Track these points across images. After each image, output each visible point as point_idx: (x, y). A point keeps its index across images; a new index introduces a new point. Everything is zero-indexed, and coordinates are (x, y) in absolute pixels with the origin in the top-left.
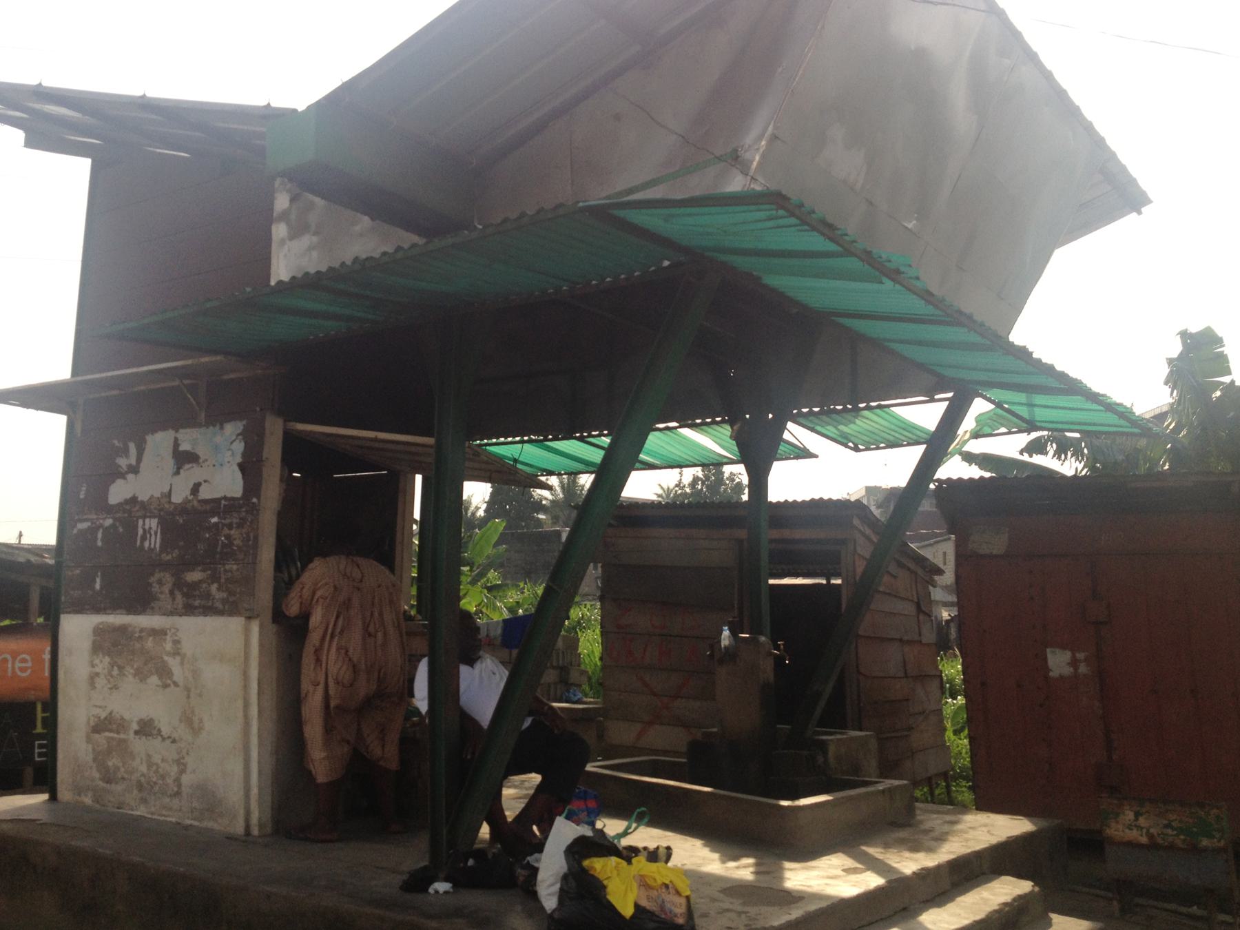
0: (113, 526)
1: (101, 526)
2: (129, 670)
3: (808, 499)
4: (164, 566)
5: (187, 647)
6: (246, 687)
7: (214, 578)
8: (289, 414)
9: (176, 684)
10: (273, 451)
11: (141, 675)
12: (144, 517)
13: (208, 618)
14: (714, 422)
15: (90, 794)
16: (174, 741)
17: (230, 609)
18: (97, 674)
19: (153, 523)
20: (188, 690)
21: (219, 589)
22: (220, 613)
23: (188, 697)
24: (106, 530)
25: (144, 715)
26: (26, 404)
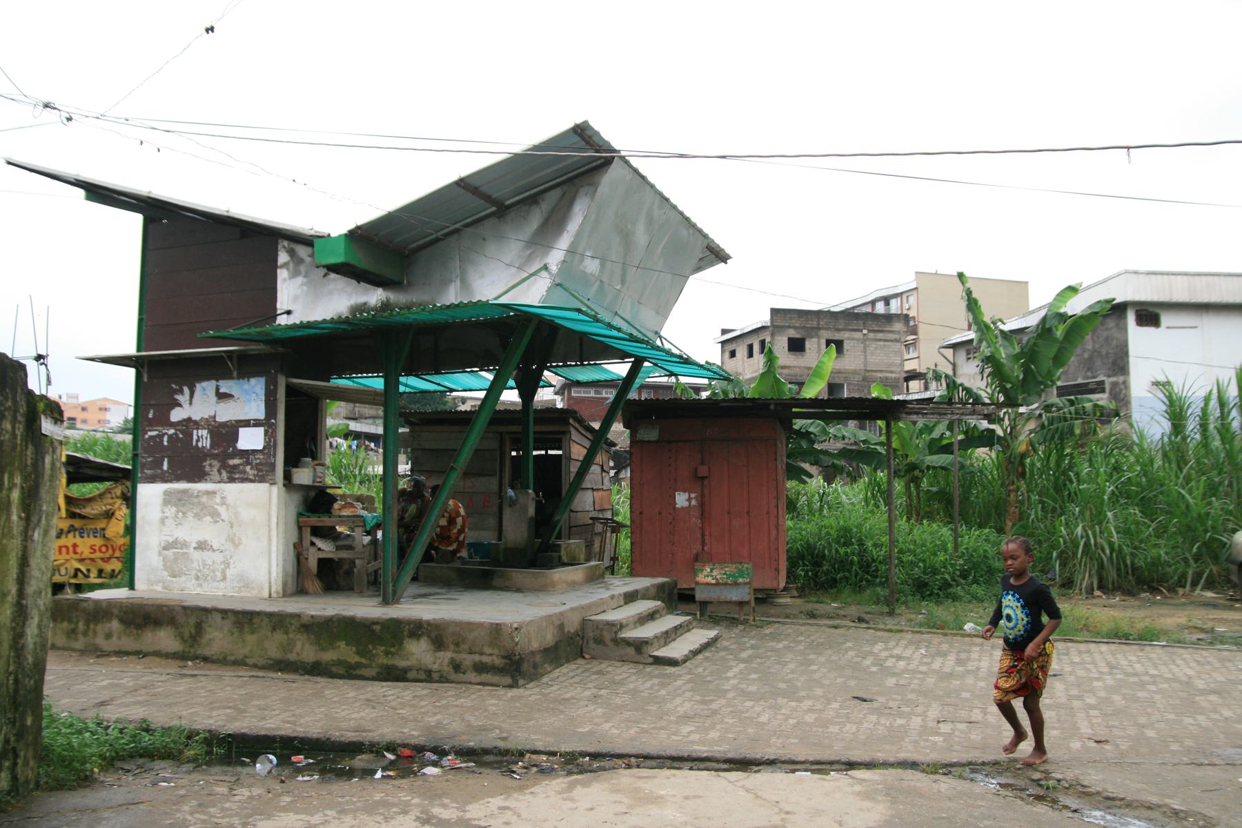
0: (175, 434)
1: (166, 434)
2: (190, 514)
4: (214, 457)
5: (229, 500)
6: (269, 520)
9: (223, 521)
12: (198, 429)
15: (160, 584)
16: (222, 552)
17: (261, 479)
18: (167, 517)
19: (204, 433)
21: (251, 469)
22: (252, 481)
23: (232, 527)
24: (170, 437)
25: (201, 539)
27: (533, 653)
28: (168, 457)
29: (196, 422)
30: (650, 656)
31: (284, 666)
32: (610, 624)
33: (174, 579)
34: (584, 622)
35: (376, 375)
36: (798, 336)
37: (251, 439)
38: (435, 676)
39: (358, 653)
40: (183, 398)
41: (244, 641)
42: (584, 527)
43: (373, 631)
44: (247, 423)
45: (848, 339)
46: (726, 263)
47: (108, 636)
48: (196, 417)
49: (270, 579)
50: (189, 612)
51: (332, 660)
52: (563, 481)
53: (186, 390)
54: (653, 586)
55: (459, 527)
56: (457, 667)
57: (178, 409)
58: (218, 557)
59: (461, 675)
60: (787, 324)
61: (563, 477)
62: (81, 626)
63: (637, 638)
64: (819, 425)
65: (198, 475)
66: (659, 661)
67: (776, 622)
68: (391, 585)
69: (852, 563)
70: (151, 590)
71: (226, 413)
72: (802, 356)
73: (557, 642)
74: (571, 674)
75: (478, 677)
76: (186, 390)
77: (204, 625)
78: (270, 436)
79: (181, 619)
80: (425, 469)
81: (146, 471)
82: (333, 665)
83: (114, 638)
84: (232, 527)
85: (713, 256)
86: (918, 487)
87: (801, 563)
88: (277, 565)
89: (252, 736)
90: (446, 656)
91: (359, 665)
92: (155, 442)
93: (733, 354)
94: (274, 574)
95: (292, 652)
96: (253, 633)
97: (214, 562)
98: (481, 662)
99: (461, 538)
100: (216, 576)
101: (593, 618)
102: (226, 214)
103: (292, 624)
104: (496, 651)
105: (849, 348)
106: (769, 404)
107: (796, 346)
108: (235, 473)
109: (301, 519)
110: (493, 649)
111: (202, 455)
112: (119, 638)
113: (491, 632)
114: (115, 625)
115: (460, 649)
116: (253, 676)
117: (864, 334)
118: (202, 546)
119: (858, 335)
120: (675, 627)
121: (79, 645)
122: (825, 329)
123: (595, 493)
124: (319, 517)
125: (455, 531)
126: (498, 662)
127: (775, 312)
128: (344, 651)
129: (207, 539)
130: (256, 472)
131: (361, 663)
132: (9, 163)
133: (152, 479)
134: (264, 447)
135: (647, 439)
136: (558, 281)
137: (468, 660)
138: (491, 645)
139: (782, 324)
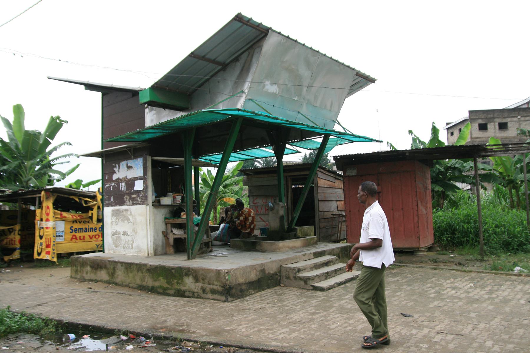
0: (115, 185)
1: (112, 185)
2: (120, 220)
3: (365, 153)
4: (127, 194)
5: (133, 213)
6: (147, 221)
7: (138, 196)
8: (152, 155)
9: (131, 222)
10: (149, 164)
11: (123, 221)
12: (121, 182)
13: (137, 206)
14: (268, 146)
15: (112, 250)
16: (131, 236)
17: (143, 203)
18: (113, 221)
19: (123, 184)
20: (134, 223)
21: (139, 199)
22: (140, 204)
23: (134, 225)
24: (113, 186)
25: (124, 230)
26: (91, 156)
27: (240, 285)
28: (113, 195)
29: (121, 180)
30: (311, 286)
31: (142, 288)
32: (293, 269)
33: (116, 248)
34: (280, 268)
35: (218, 153)
36: (483, 122)
37: (139, 186)
38: (196, 294)
39: (167, 283)
40: (116, 170)
41: (129, 276)
42: (326, 219)
43: (172, 272)
44: (137, 179)
45: (510, 121)
46: (375, 83)
47: (87, 273)
48: (121, 178)
49: (148, 247)
50: (110, 263)
51: (158, 286)
52: (315, 197)
53: (117, 165)
54: (337, 248)
55: (250, 221)
56: (204, 291)
57: (115, 174)
58: (130, 238)
59: (206, 295)
60: (477, 117)
61: (315, 196)
62: (79, 268)
63: (305, 276)
64: (460, 163)
65: (121, 203)
66: (315, 289)
67: (405, 266)
68: (190, 250)
69: (471, 232)
70: (109, 253)
71: (131, 174)
72: (486, 132)
73: (259, 279)
74: (272, 295)
75: (212, 296)
76: (117, 165)
77: (115, 268)
78: (145, 183)
79: (108, 266)
80: (254, 195)
81: (106, 202)
82: (158, 288)
83: (89, 274)
84: (134, 225)
85: (364, 80)
86: (517, 191)
87: (445, 233)
88: (150, 241)
89: (75, 324)
90: (200, 285)
91: (167, 289)
92: (108, 189)
93: (452, 134)
94: (149, 246)
95: (144, 282)
96: (131, 272)
97: (129, 241)
98: (213, 288)
99: (252, 226)
100: (130, 247)
101: (284, 266)
102: (111, 86)
103: (144, 269)
104: (219, 284)
105: (511, 126)
106: (406, 153)
107: (483, 127)
108: (134, 201)
109: (166, 220)
110: (217, 282)
111: (123, 194)
112: (90, 274)
113: (216, 274)
114: (89, 268)
115: (205, 282)
116: (118, 293)
117: (519, 119)
118: (125, 234)
119: (515, 119)
120: (335, 270)
121: (78, 277)
122: (498, 118)
123: (338, 203)
124: (173, 219)
125: (248, 223)
126: (220, 289)
127: (471, 112)
128: (162, 282)
129: (126, 230)
130: (141, 200)
131: (168, 287)
132: (49, 78)
133: (108, 205)
134: (143, 189)
135: (351, 175)
136: (249, 98)
137: (208, 287)
138: (217, 280)
139: (475, 118)
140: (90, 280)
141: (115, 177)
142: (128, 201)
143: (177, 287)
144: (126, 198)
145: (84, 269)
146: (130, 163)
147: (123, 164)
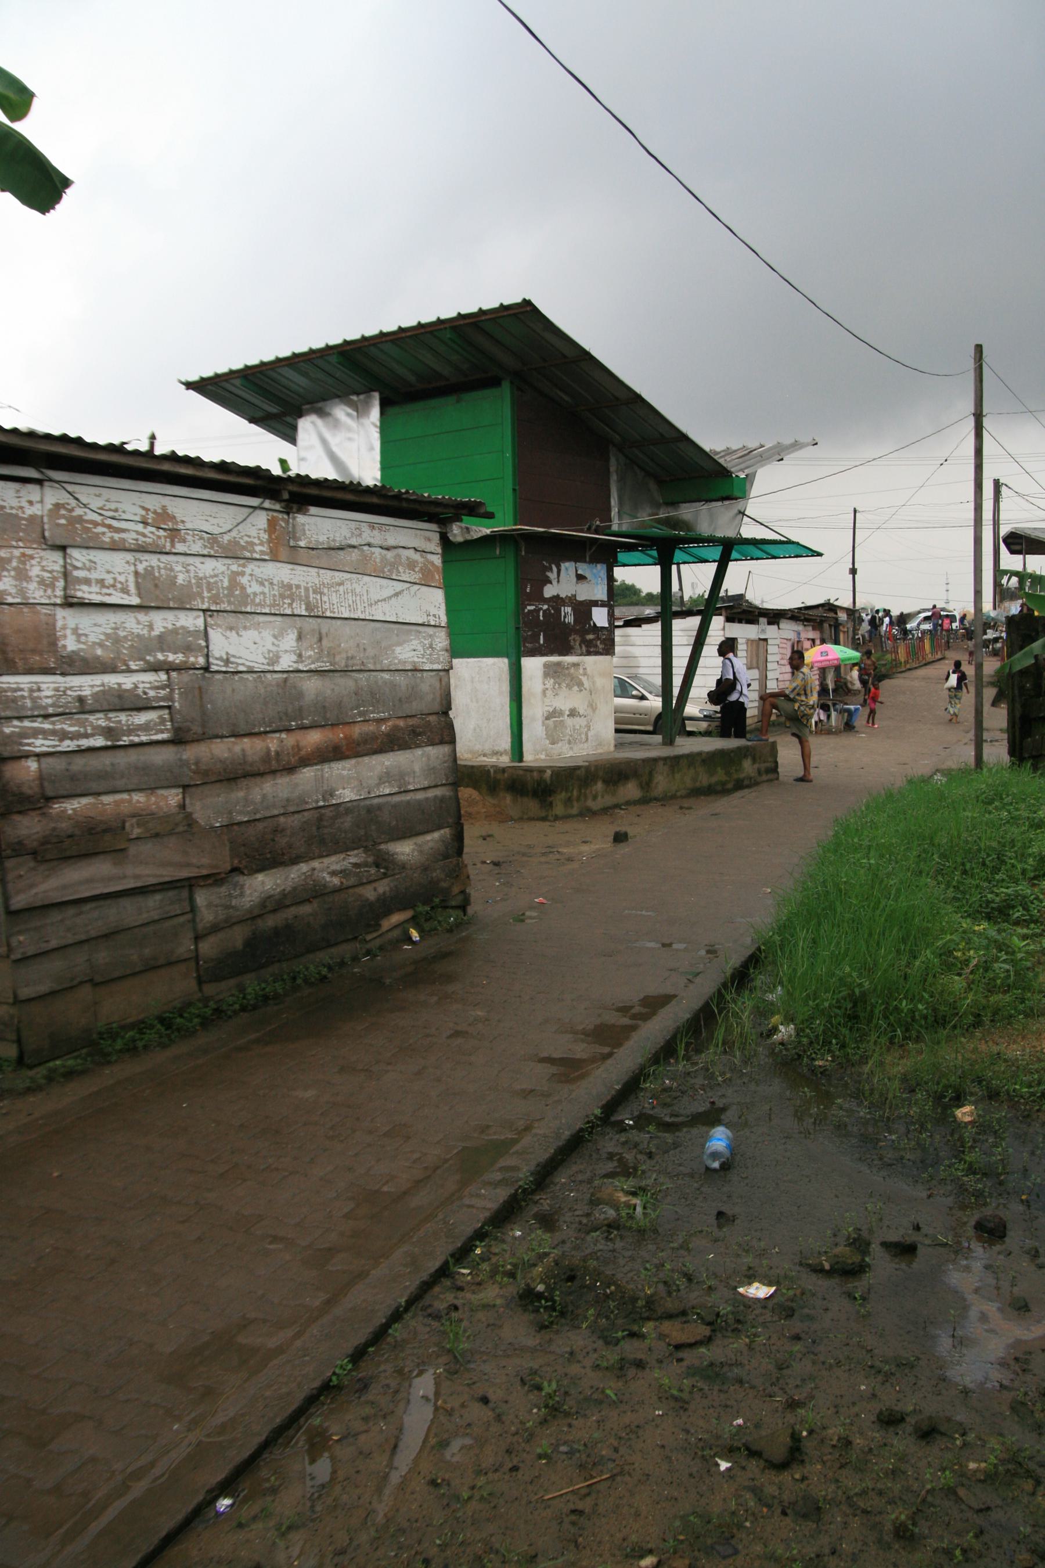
4: (576, 632)
5: (589, 671)
7: (598, 638)
19: (569, 609)
22: (601, 654)
24: (545, 611)
25: (571, 706)
40: (552, 576)
47: (595, 798)
48: (563, 595)
57: (549, 585)
58: (582, 722)
83: (599, 798)
114: (599, 786)
118: (573, 713)
121: (575, 811)
133: (532, 653)
140: (606, 810)
141: (549, 591)
142: (577, 646)
143: (735, 776)
144: (575, 639)
145: (588, 792)
146: (583, 569)
147: (568, 568)
